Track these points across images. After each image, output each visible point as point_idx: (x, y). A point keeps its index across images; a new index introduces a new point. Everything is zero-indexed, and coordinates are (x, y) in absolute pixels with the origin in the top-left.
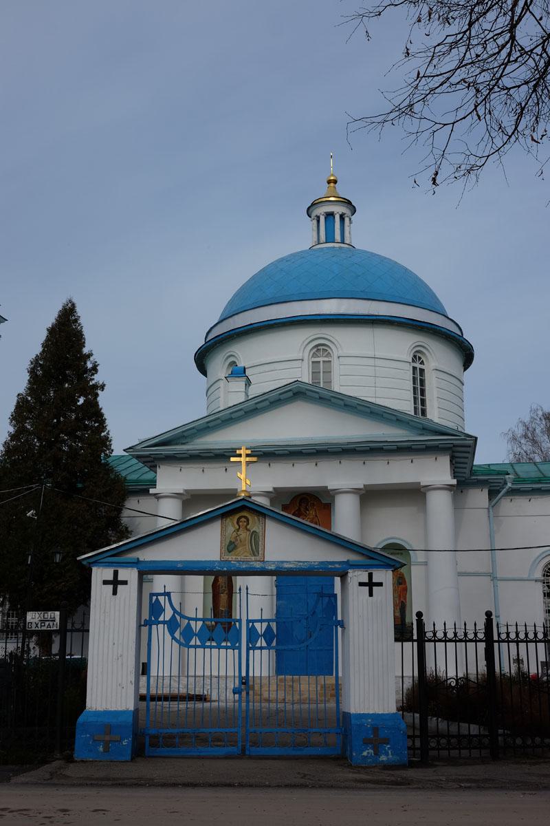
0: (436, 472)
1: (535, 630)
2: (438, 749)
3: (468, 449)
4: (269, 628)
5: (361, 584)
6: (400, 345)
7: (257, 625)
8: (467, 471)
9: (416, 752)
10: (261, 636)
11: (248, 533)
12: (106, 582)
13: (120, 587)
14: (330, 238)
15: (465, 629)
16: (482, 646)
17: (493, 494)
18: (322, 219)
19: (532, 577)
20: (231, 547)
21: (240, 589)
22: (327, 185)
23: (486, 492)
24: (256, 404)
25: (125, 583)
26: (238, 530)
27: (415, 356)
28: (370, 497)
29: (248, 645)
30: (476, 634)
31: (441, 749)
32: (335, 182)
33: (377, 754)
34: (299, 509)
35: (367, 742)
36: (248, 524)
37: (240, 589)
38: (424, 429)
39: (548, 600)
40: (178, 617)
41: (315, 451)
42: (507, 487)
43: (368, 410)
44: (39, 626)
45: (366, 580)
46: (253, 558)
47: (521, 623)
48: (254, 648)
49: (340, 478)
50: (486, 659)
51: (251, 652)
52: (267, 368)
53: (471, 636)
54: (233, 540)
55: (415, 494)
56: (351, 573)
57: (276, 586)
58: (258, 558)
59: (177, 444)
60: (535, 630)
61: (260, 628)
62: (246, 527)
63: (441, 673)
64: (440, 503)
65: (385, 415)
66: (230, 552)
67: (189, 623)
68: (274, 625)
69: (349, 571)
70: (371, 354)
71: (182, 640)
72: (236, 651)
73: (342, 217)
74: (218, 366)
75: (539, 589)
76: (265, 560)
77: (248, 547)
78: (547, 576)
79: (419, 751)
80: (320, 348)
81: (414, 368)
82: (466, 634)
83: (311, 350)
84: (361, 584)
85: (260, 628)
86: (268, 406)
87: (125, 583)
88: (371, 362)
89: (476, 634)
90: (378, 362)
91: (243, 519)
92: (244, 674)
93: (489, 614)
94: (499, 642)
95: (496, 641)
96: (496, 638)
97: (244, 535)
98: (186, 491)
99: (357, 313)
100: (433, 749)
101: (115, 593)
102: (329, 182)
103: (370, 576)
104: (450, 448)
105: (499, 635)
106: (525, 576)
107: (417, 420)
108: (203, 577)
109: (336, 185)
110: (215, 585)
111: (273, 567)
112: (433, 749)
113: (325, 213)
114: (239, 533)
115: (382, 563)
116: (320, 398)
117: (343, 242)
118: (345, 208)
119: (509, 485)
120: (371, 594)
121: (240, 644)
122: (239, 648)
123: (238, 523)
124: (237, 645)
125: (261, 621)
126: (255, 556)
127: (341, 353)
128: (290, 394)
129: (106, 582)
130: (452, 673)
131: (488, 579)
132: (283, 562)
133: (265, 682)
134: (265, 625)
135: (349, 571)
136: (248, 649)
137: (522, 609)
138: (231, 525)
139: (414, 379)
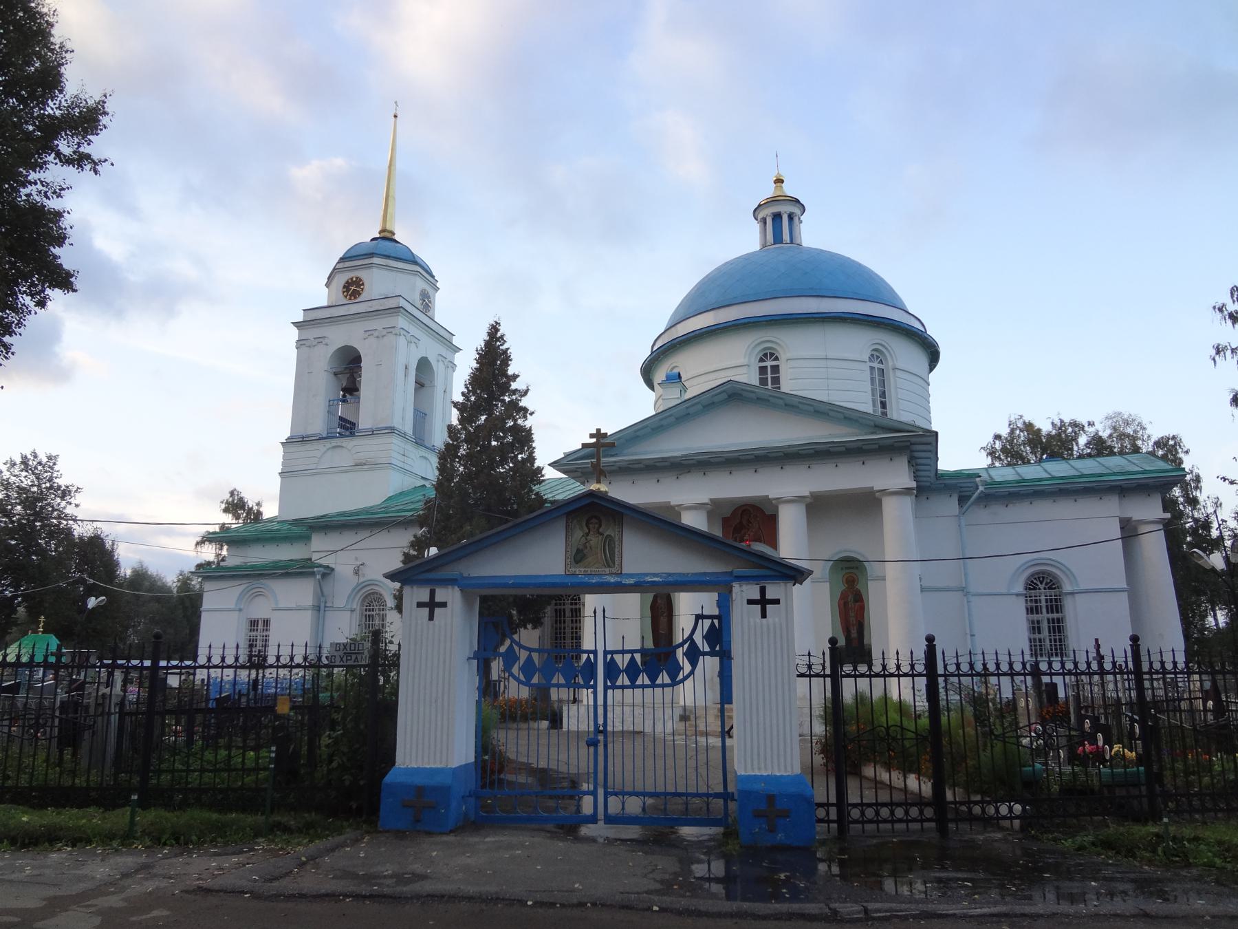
0: (893, 476)
2: (863, 823)
3: (929, 447)
5: (750, 602)
6: (858, 343)
7: (618, 658)
13: (437, 610)
14: (778, 239)
16: (922, 682)
17: (962, 500)
18: (769, 221)
23: (955, 499)
25: (444, 605)
26: (587, 534)
28: (819, 507)
30: (912, 666)
40: (516, 648)
43: (811, 409)
45: (426, 599)
46: (607, 570)
48: (614, 687)
50: (928, 700)
51: (610, 692)
56: (736, 588)
61: (622, 661)
65: (831, 413)
67: (530, 656)
70: (821, 354)
71: (522, 677)
72: (590, 690)
74: (659, 376)
79: (835, 825)
81: (872, 368)
82: (898, 667)
84: (750, 602)
85: (622, 661)
87: (444, 605)
89: (912, 666)
90: (830, 363)
91: (594, 520)
95: (941, 675)
96: (940, 670)
97: (594, 540)
100: (856, 822)
101: (431, 618)
104: (907, 448)
105: (945, 667)
106: (1004, 591)
107: (880, 424)
108: (639, 595)
112: (856, 822)
119: (981, 488)
120: (764, 615)
121: (596, 682)
122: (595, 687)
126: (609, 566)
127: (789, 355)
129: (420, 605)
130: (700, 702)
131: (960, 594)
132: (647, 575)
133: (701, 713)
134: (628, 657)
136: (606, 688)
139: (872, 380)
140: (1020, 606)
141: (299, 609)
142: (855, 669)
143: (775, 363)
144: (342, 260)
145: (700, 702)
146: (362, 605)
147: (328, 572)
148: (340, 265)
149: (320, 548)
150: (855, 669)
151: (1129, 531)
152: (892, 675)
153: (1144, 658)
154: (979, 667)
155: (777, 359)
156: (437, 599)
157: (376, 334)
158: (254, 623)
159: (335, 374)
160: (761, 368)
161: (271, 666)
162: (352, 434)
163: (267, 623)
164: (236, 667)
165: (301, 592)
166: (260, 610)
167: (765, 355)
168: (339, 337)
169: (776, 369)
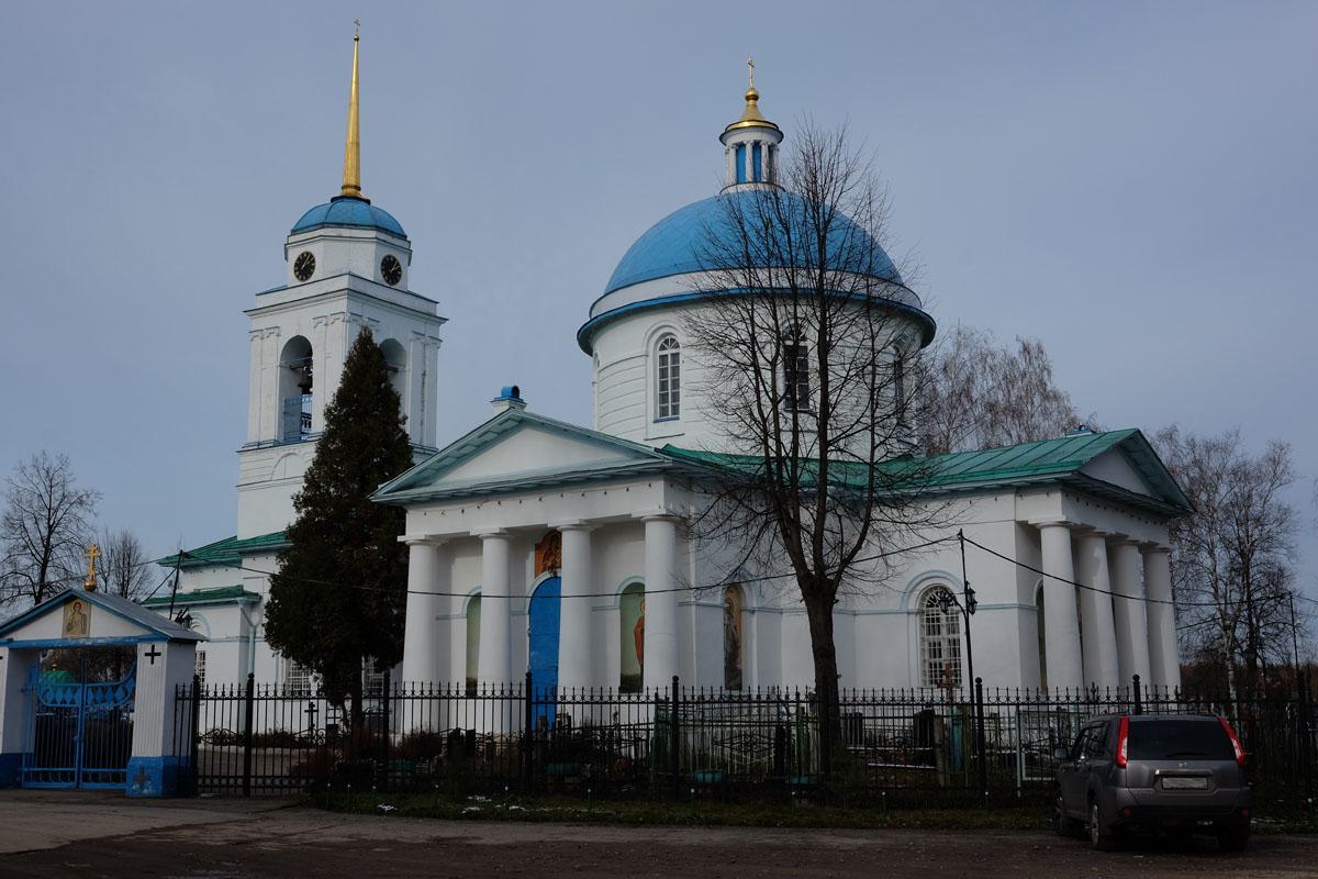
12: (147, 654)
18: (749, 148)
20: (69, 627)
22: (745, 101)
25: (159, 654)
32: (755, 98)
33: (142, 787)
34: (550, 549)
35: (135, 779)
52: (614, 368)
57: (530, 635)
59: (421, 486)
63: (287, 729)
77: (80, 628)
82: (1108, 698)
83: (657, 342)
86: (496, 438)
87: (159, 654)
94: (520, 699)
96: (255, 696)
97: (78, 617)
98: (586, 521)
99: (666, 294)
102: (748, 98)
106: (897, 608)
109: (757, 102)
113: (736, 144)
118: (760, 134)
129: (147, 654)
130: (497, 731)
138: (70, 608)
140: (914, 626)
141: (229, 640)
142: (629, 698)
143: (674, 351)
144: (294, 232)
145: (497, 731)
148: (292, 239)
150: (629, 698)
151: (1031, 534)
152: (606, 703)
153: (680, 692)
154: (869, 699)
155: (677, 346)
156: (156, 651)
160: (661, 357)
161: (1103, 703)
164: (1078, 704)
167: (666, 342)
168: (292, 324)
169: (675, 357)
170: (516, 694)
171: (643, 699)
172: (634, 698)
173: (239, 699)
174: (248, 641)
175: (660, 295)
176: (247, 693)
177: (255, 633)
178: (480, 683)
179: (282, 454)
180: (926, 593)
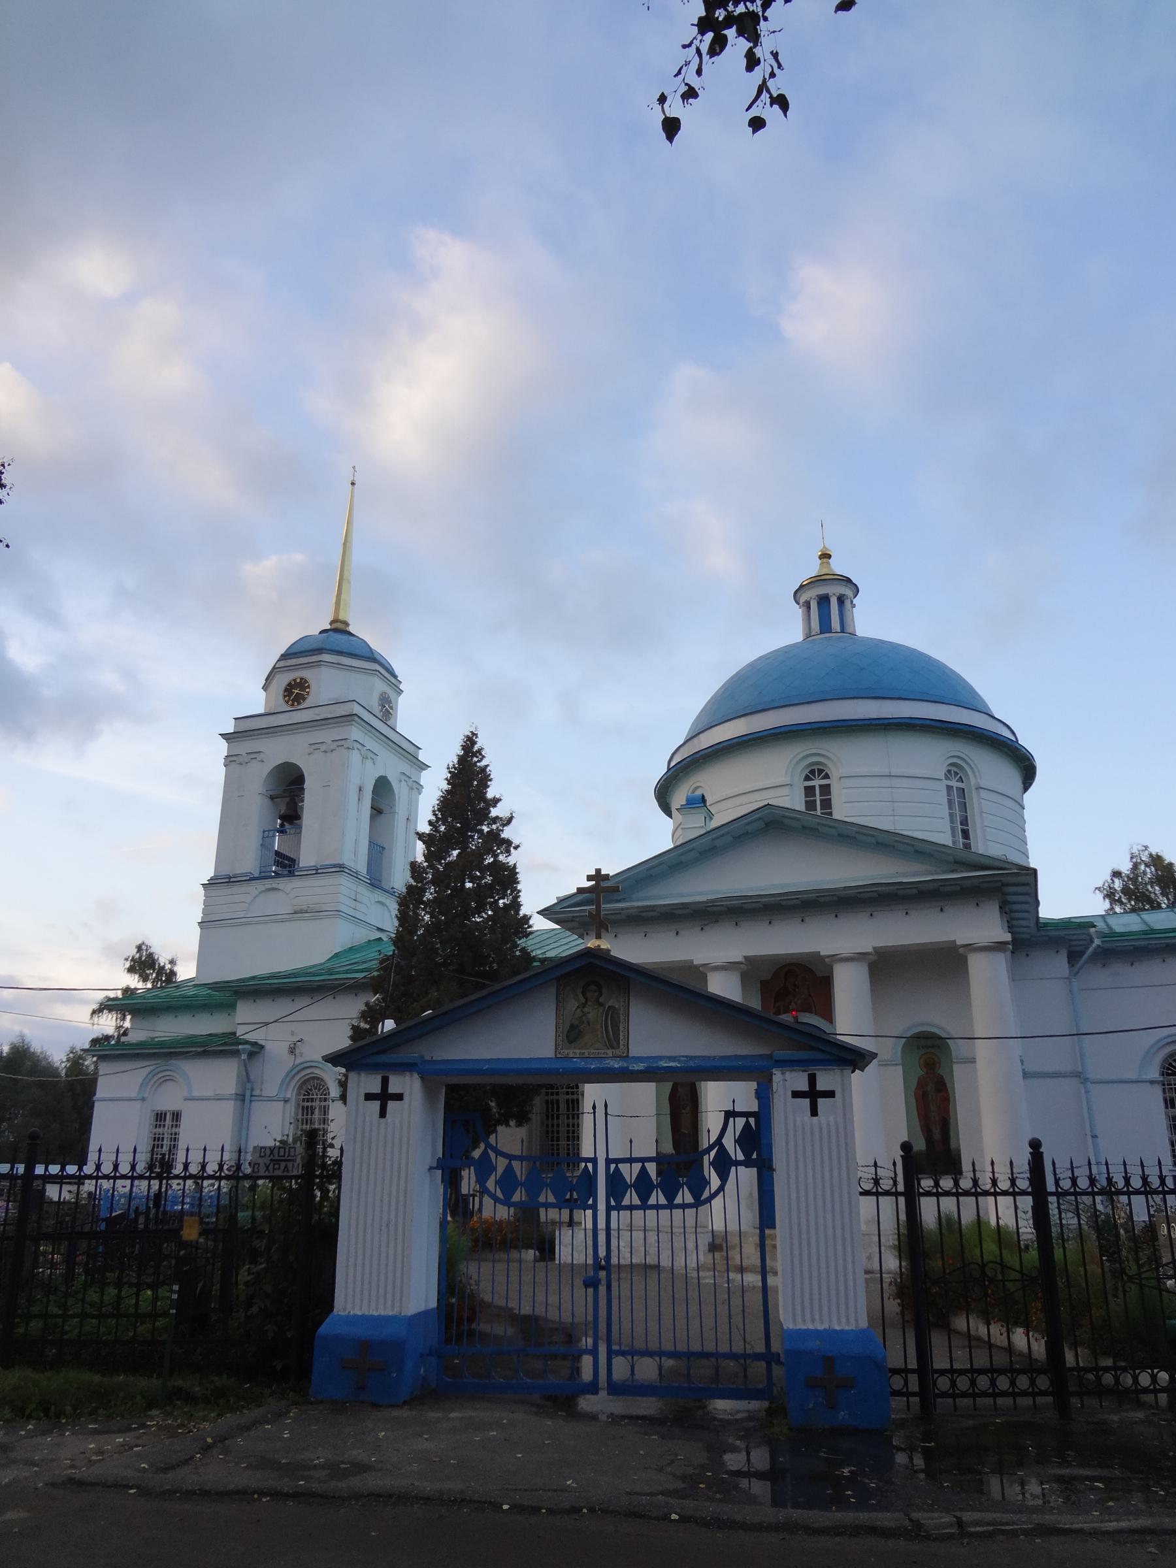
0: (981, 926)
1: (1126, 1172)
4: (643, 1172)
5: (796, 1094)
7: (624, 1168)
8: (1032, 923)
9: (911, 1399)
10: (631, 1186)
11: (601, 1010)
14: (825, 627)
15: (993, 1172)
16: (1027, 1202)
18: (814, 605)
19: (1145, 1077)
21: (594, 1107)
24: (713, 840)
26: (584, 1005)
27: (949, 771)
28: (885, 967)
29: (608, 1202)
31: (958, 1396)
36: (600, 995)
37: (594, 1107)
38: (956, 862)
39: (1172, 1112)
40: (492, 1155)
41: (798, 902)
42: (1094, 945)
44: (271, 1167)
45: (804, 1086)
46: (610, 1052)
47: (1079, 1161)
48: (619, 1208)
49: (840, 940)
51: (614, 1214)
53: (1004, 1185)
54: (576, 1022)
55: (947, 963)
58: (618, 1052)
60: (1126, 1172)
61: (629, 1172)
62: (597, 1000)
64: (988, 976)
66: (570, 1042)
68: (652, 1168)
69: (774, 1071)
70: (885, 771)
71: (499, 1194)
73: (841, 600)
74: (678, 799)
75: (1154, 1099)
76: (631, 1055)
78: (1168, 1074)
80: (816, 771)
81: (949, 788)
82: (994, 1182)
84: (796, 1094)
85: (629, 1172)
87: (399, 1097)
88: (886, 782)
89: (1013, 1181)
90: (896, 782)
91: (593, 987)
92: (602, 1252)
93: (1035, 1145)
96: (1051, 1187)
97: (592, 1013)
100: (944, 1395)
101: (383, 1114)
103: (812, 1080)
106: (1134, 1077)
107: (961, 858)
110: (674, 1099)
111: (641, 1066)
112: (944, 1395)
114: (586, 1010)
115: (828, 1057)
116: (804, 827)
117: (843, 631)
119: (1097, 942)
120: (814, 1112)
121: (595, 1201)
122: (594, 1208)
123: (584, 994)
124: (590, 1202)
125: (631, 1160)
126: (612, 1047)
128: (761, 824)
129: (369, 1097)
134: (637, 1167)
135: (774, 1071)
136: (609, 1209)
137: (1127, 1136)
141: (218, 1098)
142: (937, 1185)
144: (284, 657)
145: (733, 1227)
146: (299, 1094)
147: (256, 1050)
149: (246, 1020)
152: (986, 1193)
155: (827, 776)
157: (323, 748)
158: (160, 1117)
159: (272, 798)
162: (291, 874)
163: (177, 1116)
165: (220, 1077)
166: (169, 1099)
168: (277, 751)
169: (826, 789)
170: (886, 1185)
171: (966, 1184)
172: (72, 1169)
173: (1014, 1193)
174: (243, 1100)
175: (861, 717)
176: (1031, 1181)
177: (252, 1090)
178: (182, 1145)
179: (263, 888)
180: (304, 1083)
